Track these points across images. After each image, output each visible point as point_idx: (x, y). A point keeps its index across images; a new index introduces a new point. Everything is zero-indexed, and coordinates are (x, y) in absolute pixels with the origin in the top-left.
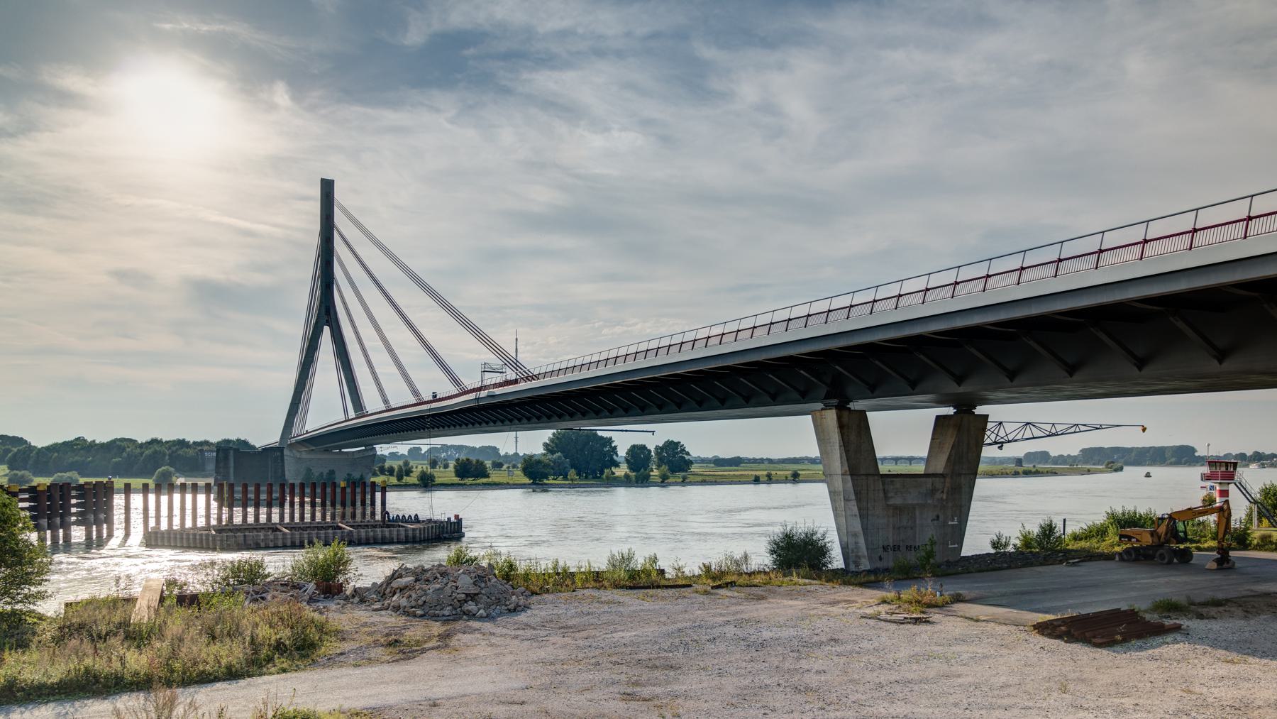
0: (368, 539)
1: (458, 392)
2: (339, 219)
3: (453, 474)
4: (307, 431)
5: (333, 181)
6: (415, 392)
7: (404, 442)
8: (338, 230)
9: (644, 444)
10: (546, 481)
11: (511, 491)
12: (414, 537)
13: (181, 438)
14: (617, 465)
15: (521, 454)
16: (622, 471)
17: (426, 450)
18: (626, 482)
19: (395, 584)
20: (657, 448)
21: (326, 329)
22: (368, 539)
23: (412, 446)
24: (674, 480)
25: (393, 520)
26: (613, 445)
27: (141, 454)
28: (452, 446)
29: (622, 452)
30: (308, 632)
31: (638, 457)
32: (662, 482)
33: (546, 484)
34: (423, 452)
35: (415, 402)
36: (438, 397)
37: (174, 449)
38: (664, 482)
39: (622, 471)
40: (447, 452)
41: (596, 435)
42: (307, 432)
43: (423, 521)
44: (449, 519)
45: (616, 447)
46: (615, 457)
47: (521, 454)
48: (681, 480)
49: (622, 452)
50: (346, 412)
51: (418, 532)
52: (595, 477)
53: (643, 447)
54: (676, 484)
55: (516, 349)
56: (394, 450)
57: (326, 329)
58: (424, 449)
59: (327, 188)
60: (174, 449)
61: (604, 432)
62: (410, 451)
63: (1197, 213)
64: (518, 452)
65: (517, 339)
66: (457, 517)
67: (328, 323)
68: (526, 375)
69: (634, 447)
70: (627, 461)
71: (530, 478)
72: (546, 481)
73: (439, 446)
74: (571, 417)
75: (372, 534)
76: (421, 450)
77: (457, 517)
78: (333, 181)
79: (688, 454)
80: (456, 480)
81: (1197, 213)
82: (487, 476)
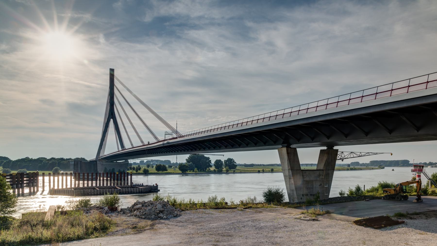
0: (126, 192)
3: (155, 170)
5: (114, 69)
7: (138, 159)
9: (220, 159)
10: (187, 172)
11: (175, 175)
12: (142, 191)
13: (62, 157)
14: (211, 166)
15: (178, 163)
16: (213, 169)
18: (214, 172)
19: (135, 207)
20: (225, 161)
21: (112, 120)
22: (126, 192)
23: (141, 160)
24: (231, 172)
25: (134, 185)
26: (210, 160)
27: (48, 163)
29: (213, 162)
31: (218, 164)
32: (227, 172)
33: (187, 173)
34: (145, 162)
36: (150, 143)
37: (60, 161)
38: (227, 172)
39: (213, 169)
41: (204, 156)
42: (105, 155)
43: (145, 186)
44: (154, 185)
45: (211, 160)
46: (210, 164)
47: (178, 163)
48: (233, 172)
49: (213, 162)
50: (118, 148)
51: (143, 189)
52: (204, 171)
53: (220, 161)
54: (231, 173)
55: (177, 127)
57: (112, 120)
58: (145, 161)
60: (60, 161)
61: (206, 155)
62: (140, 162)
66: (156, 184)
67: (112, 118)
69: (217, 160)
70: (215, 165)
71: (181, 171)
72: (187, 172)
73: (150, 160)
75: (127, 190)
77: (156, 184)
78: (114, 69)
79: (235, 163)
80: (156, 172)
82: (167, 170)
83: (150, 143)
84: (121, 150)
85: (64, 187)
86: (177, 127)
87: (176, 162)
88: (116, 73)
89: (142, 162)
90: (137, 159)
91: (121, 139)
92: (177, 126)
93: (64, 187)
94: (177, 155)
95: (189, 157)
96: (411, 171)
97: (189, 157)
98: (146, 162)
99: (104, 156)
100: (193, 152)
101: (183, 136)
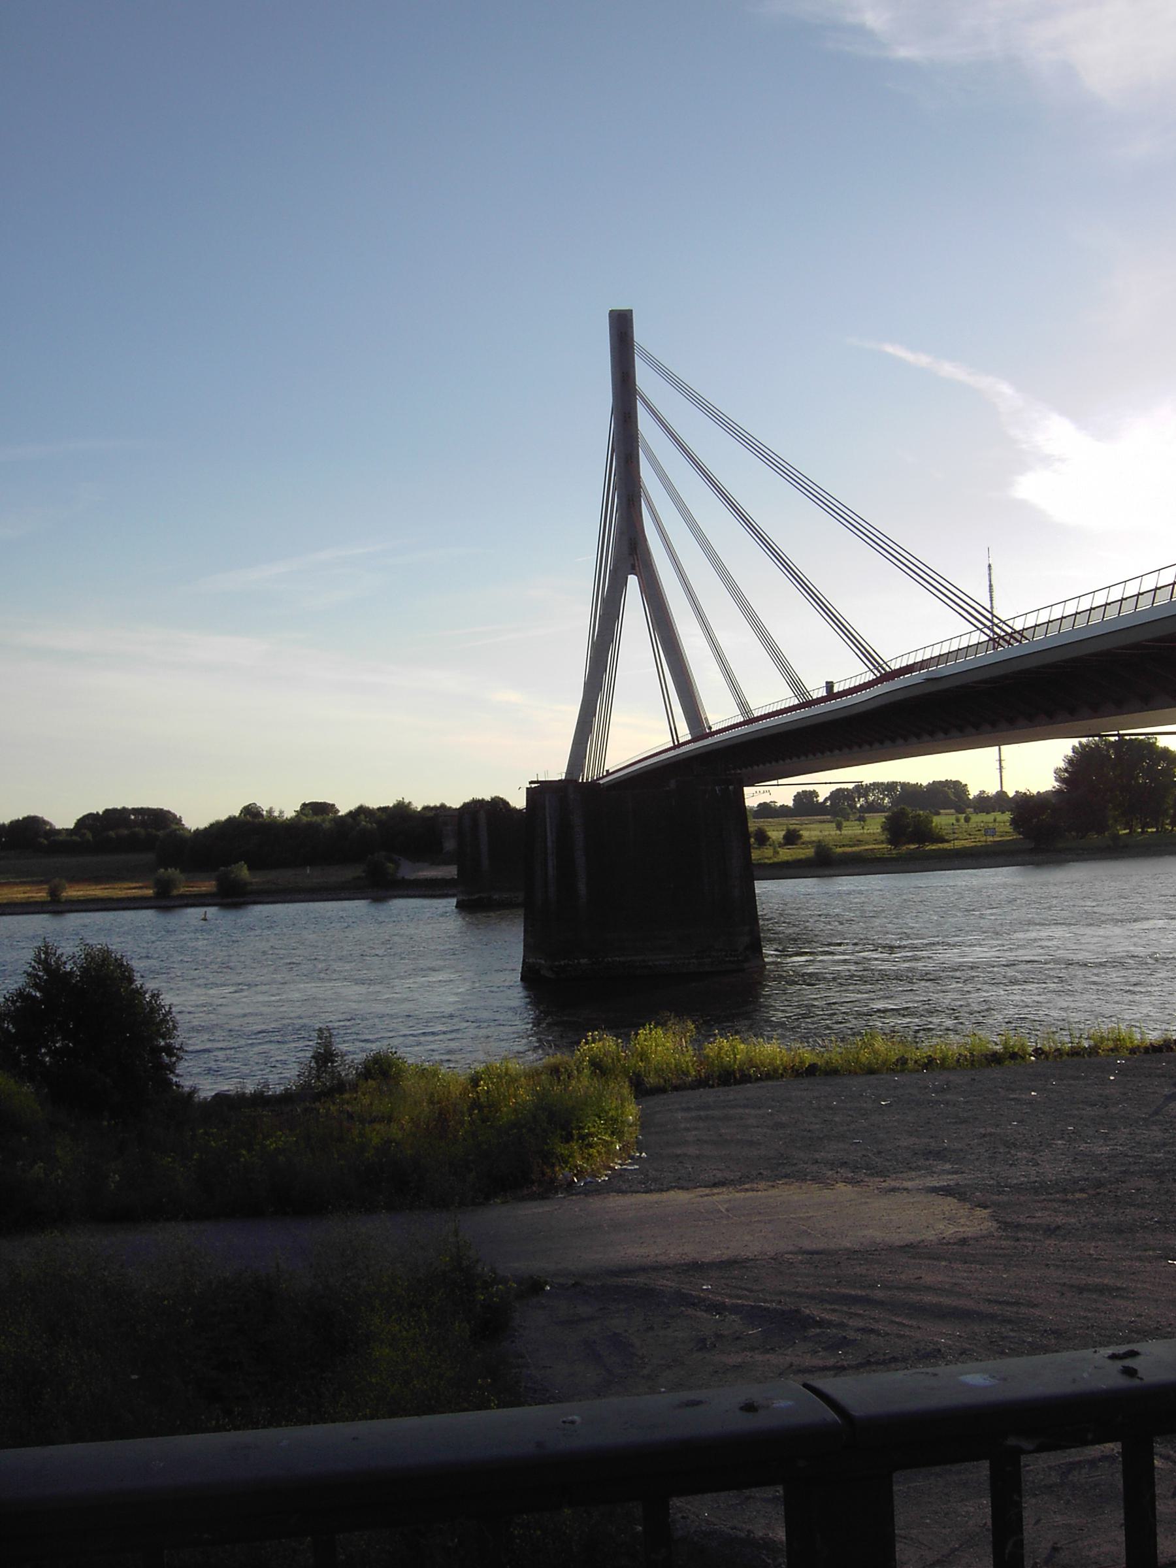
1: (872, 677)
2: (645, 423)
4: (607, 771)
5: (632, 310)
6: (795, 684)
7: (781, 781)
8: (642, 398)
15: (1011, 794)
17: (828, 795)
21: (633, 581)
23: (800, 789)
28: (876, 786)
30: (616, 1160)
34: (821, 799)
35: (870, 677)
36: (835, 690)
40: (866, 796)
41: (1153, 745)
42: (608, 774)
47: (1011, 794)
50: (673, 731)
55: (991, 586)
56: (766, 799)
57: (633, 581)
58: (824, 793)
59: (621, 325)
62: (799, 798)
63: (1155, 594)
64: (1004, 789)
65: (990, 566)
68: (1003, 634)
73: (851, 786)
74: (946, 734)
76: (817, 796)
78: (632, 310)
81: (1155, 594)
83: (835, 690)
84: (689, 737)
85: (585, 781)
86: (991, 586)
87: (999, 789)
88: (641, 335)
89: (805, 801)
90: (775, 782)
91: (1084, 734)
92: (990, 581)
93: (585, 781)
94: (1004, 748)
95: (1070, 754)
96: (829, 680)
97: (1070, 754)
98: (826, 800)
99: (604, 777)
100: (1080, 722)
101: (1018, 632)
